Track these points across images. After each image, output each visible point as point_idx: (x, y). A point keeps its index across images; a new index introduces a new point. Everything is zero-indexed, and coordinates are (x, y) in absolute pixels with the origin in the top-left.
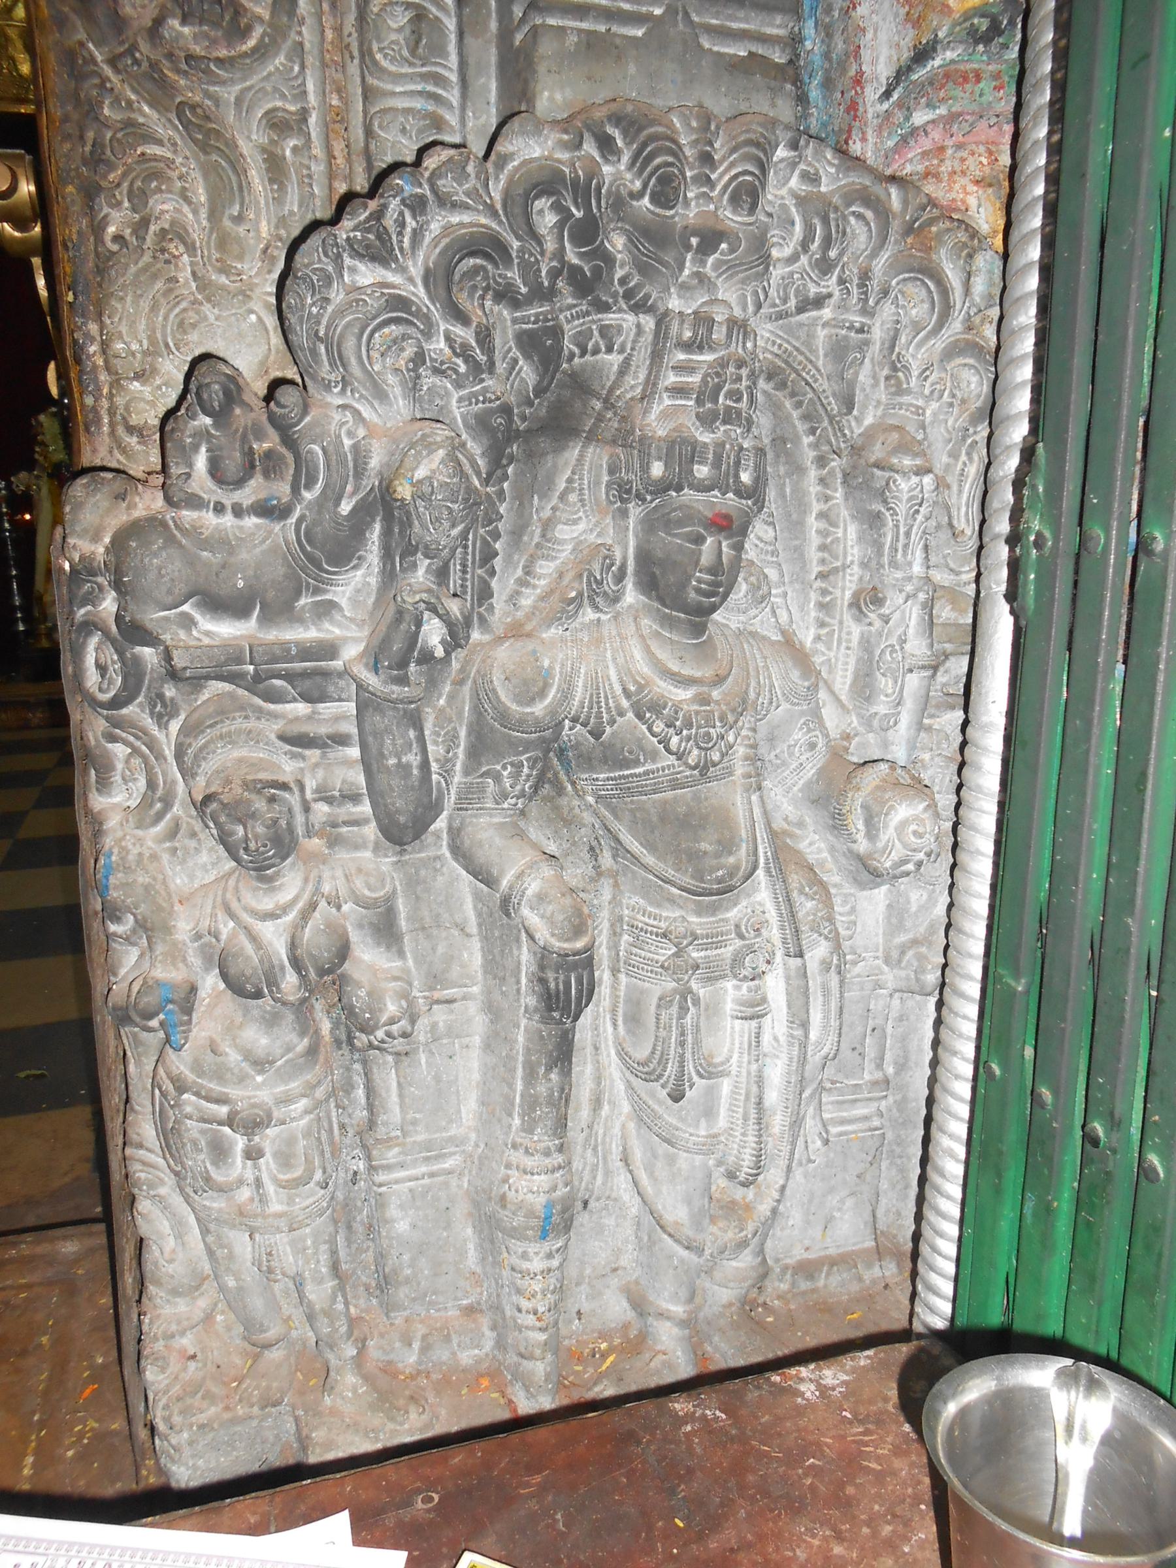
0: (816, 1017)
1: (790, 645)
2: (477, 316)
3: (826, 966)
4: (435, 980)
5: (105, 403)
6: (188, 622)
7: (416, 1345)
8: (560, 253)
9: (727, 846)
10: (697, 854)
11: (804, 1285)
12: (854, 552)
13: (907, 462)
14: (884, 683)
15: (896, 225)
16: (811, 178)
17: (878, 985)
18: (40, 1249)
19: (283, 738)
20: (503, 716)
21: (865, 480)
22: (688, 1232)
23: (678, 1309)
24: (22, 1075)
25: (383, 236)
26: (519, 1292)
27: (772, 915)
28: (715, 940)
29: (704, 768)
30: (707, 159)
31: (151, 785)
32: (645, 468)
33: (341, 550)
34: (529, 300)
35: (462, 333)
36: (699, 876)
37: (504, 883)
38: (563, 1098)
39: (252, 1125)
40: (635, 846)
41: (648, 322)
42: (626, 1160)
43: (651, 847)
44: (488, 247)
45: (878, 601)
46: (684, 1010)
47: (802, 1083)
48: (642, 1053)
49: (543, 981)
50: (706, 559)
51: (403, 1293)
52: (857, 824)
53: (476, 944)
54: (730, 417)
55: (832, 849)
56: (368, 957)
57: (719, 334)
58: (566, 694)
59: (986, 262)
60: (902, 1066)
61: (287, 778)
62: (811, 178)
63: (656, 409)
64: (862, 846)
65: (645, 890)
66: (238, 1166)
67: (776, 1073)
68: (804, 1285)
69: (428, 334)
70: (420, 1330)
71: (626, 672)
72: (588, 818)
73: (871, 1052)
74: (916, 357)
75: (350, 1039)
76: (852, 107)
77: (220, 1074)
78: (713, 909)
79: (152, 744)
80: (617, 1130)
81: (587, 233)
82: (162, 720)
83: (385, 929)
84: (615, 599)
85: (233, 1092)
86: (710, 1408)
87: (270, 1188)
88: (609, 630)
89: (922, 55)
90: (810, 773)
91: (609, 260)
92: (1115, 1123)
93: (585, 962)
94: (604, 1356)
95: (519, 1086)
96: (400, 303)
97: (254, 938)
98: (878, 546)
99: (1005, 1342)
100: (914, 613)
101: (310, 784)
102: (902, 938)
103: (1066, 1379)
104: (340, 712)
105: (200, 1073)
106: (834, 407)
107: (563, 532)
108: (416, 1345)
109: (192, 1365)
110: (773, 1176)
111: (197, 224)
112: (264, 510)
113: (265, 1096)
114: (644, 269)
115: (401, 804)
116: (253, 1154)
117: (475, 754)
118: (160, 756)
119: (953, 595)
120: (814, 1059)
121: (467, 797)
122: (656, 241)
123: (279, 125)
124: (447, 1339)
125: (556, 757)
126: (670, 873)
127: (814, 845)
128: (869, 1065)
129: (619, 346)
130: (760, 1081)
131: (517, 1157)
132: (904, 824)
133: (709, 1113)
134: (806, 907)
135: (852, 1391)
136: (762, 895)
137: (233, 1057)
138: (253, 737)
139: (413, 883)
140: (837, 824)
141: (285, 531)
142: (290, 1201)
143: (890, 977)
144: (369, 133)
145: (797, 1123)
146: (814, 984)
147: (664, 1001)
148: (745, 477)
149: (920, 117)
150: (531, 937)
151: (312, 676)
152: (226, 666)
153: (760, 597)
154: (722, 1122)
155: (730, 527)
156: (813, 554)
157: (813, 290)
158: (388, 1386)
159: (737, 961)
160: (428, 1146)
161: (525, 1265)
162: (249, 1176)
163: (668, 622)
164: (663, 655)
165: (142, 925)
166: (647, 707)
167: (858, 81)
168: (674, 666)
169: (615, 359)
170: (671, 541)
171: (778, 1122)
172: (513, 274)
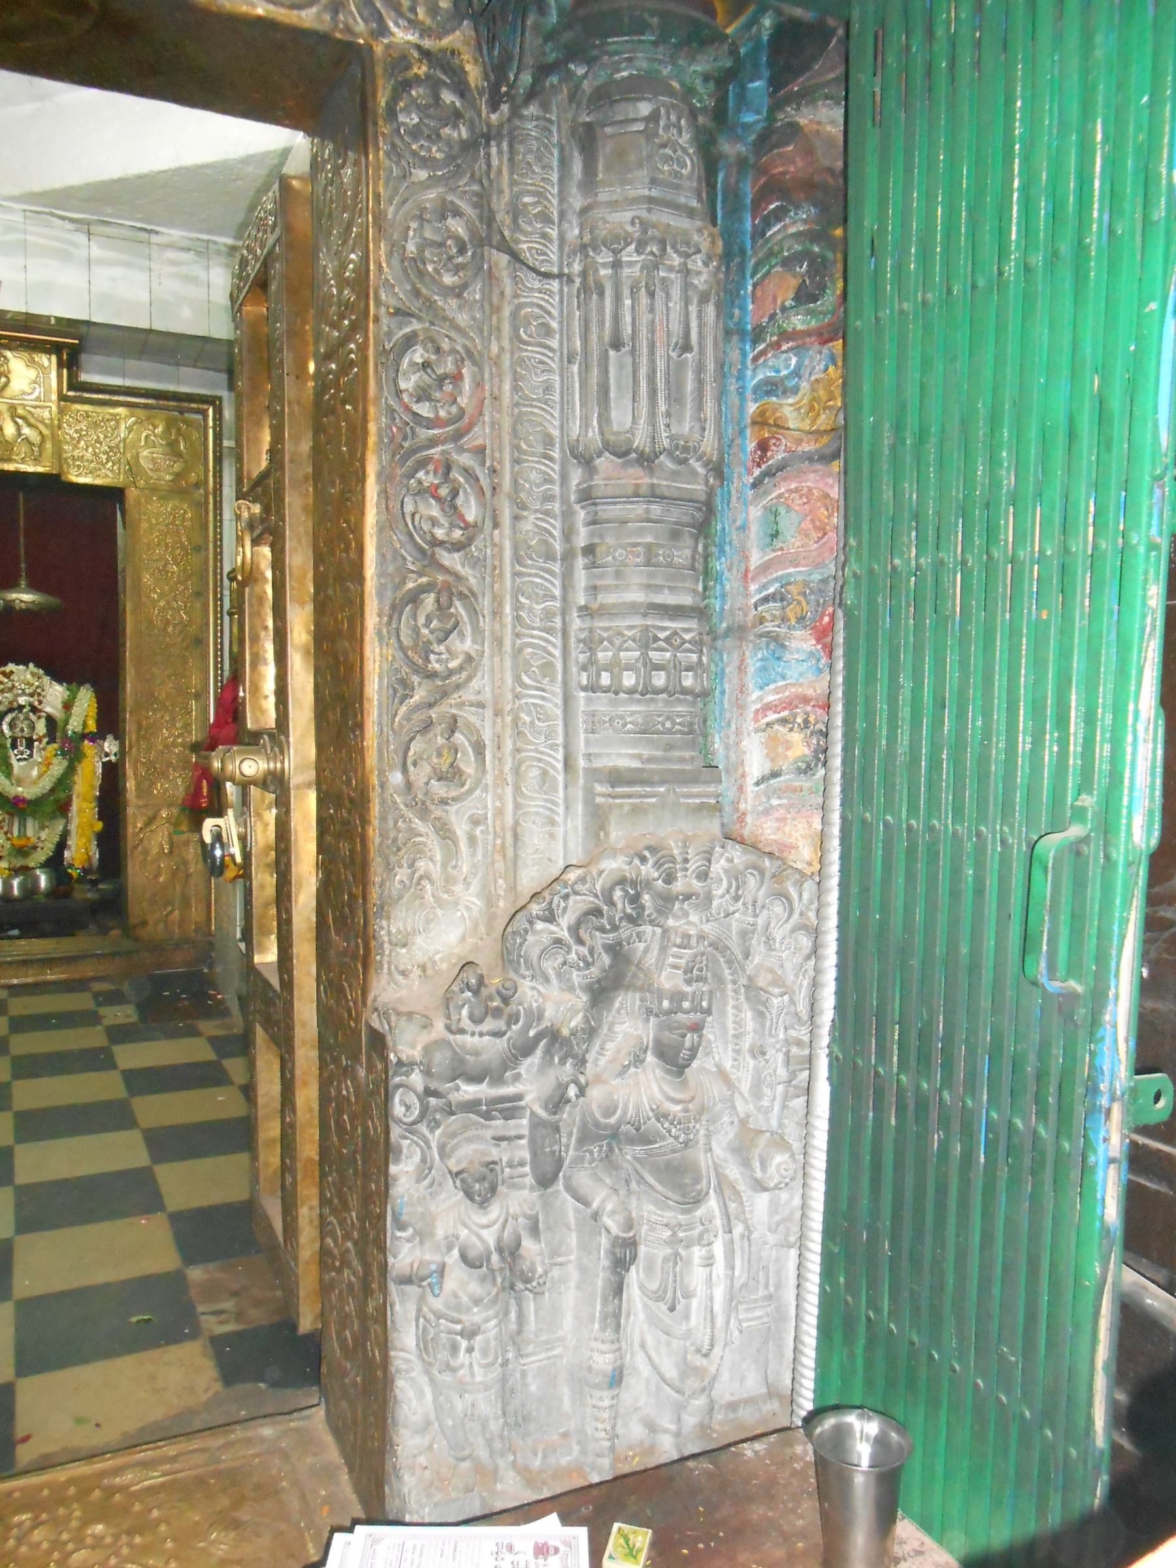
0: (738, 1263)
1: (722, 1074)
2: (588, 941)
3: (742, 1237)
4: (555, 1253)
5: (386, 959)
6: (458, 1089)
7: (540, 1455)
8: (624, 910)
9: (697, 1180)
10: (682, 1182)
11: (732, 1416)
12: (750, 1025)
13: (776, 991)
14: (767, 1091)
15: (768, 874)
16: (730, 860)
17: (765, 1243)
18: (249, 1434)
19: (494, 1138)
20: (597, 1124)
21: (754, 993)
22: (677, 1383)
23: (673, 1427)
24: (134, 1319)
25: (552, 912)
26: (597, 1419)
27: (717, 1213)
28: (690, 1227)
29: (686, 1144)
30: (686, 861)
31: (424, 1160)
32: (660, 1003)
33: (526, 1050)
34: (610, 931)
35: (584, 950)
36: (684, 1196)
37: (595, 1205)
38: (617, 1315)
39: (470, 1333)
40: (651, 1181)
41: (659, 930)
42: (643, 1346)
43: (661, 1182)
44: (597, 912)
45: (763, 1053)
46: (676, 1263)
47: (731, 1300)
48: (654, 1286)
49: (614, 1253)
50: (688, 1044)
51: (532, 1426)
52: (757, 1164)
53: (574, 1235)
54: (699, 979)
55: (742, 1174)
56: (528, 1244)
57: (693, 942)
58: (625, 1112)
59: (809, 887)
60: (778, 1286)
61: (496, 1159)
62: (730, 860)
63: (664, 973)
64: (759, 1174)
65: (656, 1203)
66: (462, 1356)
67: (719, 1294)
68: (732, 1416)
69: (569, 952)
70: (541, 1447)
71: (651, 1098)
72: (625, 1165)
73: (762, 1279)
74: (778, 934)
75: (512, 1287)
76: (741, 788)
77: (458, 1308)
78: (688, 1211)
79: (427, 1142)
80: (637, 1330)
81: (635, 900)
82: (432, 1130)
83: (535, 1231)
84: (643, 1061)
85: (464, 1317)
86: (706, 1465)
87: (476, 1368)
88: (642, 1077)
89: (775, 774)
90: (731, 1136)
91: (643, 908)
92: (878, 1311)
93: (632, 1244)
94: (633, 1457)
95: (599, 1307)
96: (558, 942)
97: (479, 1237)
98: (763, 1026)
99: (837, 1408)
100: (780, 1057)
101: (505, 1159)
102: (777, 1218)
103: (861, 1417)
104: (523, 1124)
105: (449, 1308)
106: (740, 957)
107: (618, 1028)
108: (540, 1455)
109: (427, 1472)
110: (717, 1351)
111: (436, 871)
112: (498, 1034)
113: (477, 1319)
114: (659, 912)
115: (549, 1168)
116: (470, 1350)
117: (581, 1142)
118: (429, 1147)
119: (799, 1043)
120: (737, 1285)
121: (578, 1161)
122: (666, 901)
123: (475, 822)
124: (555, 1451)
125: (609, 1137)
126: (670, 1194)
127: (733, 1172)
128: (761, 1288)
129: (646, 944)
130: (711, 1299)
131: (595, 1345)
132: (779, 1166)
133: (687, 1317)
134: (733, 1206)
135: (769, 1452)
136: (712, 1203)
137: (465, 1299)
138: (481, 1139)
139: (546, 1205)
140: (746, 1163)
141: (501, 1044)
142: (486, 1375)
143: (772, 1239)
144: (517, 823)
145: (728, 1322)
146: (737, 1246)
147: (666, 1260)
148: (704, 1004)
149: (775, 802)
150: (608, 1231)
151: (509, 1108)
152: (472, 1106)
153: (708, 1053)
154: (693, 1321)
155: (697, 1028)
156: (730, 1025)
157: (731, 909)
158: (529, 1477)
159: (701, 1237)
160: (547, 1342)
161: (601, 1404)
162: (467, 1363)
163: (668, 1072)
164: (666, 1088)
165: (418, 1233)
166: (661, 1116)
167: (743, 776)
168: (672, 1094)
169: (642, 946)
170: (670, 1037)
171: (720, 1321)
172: (604, 921)
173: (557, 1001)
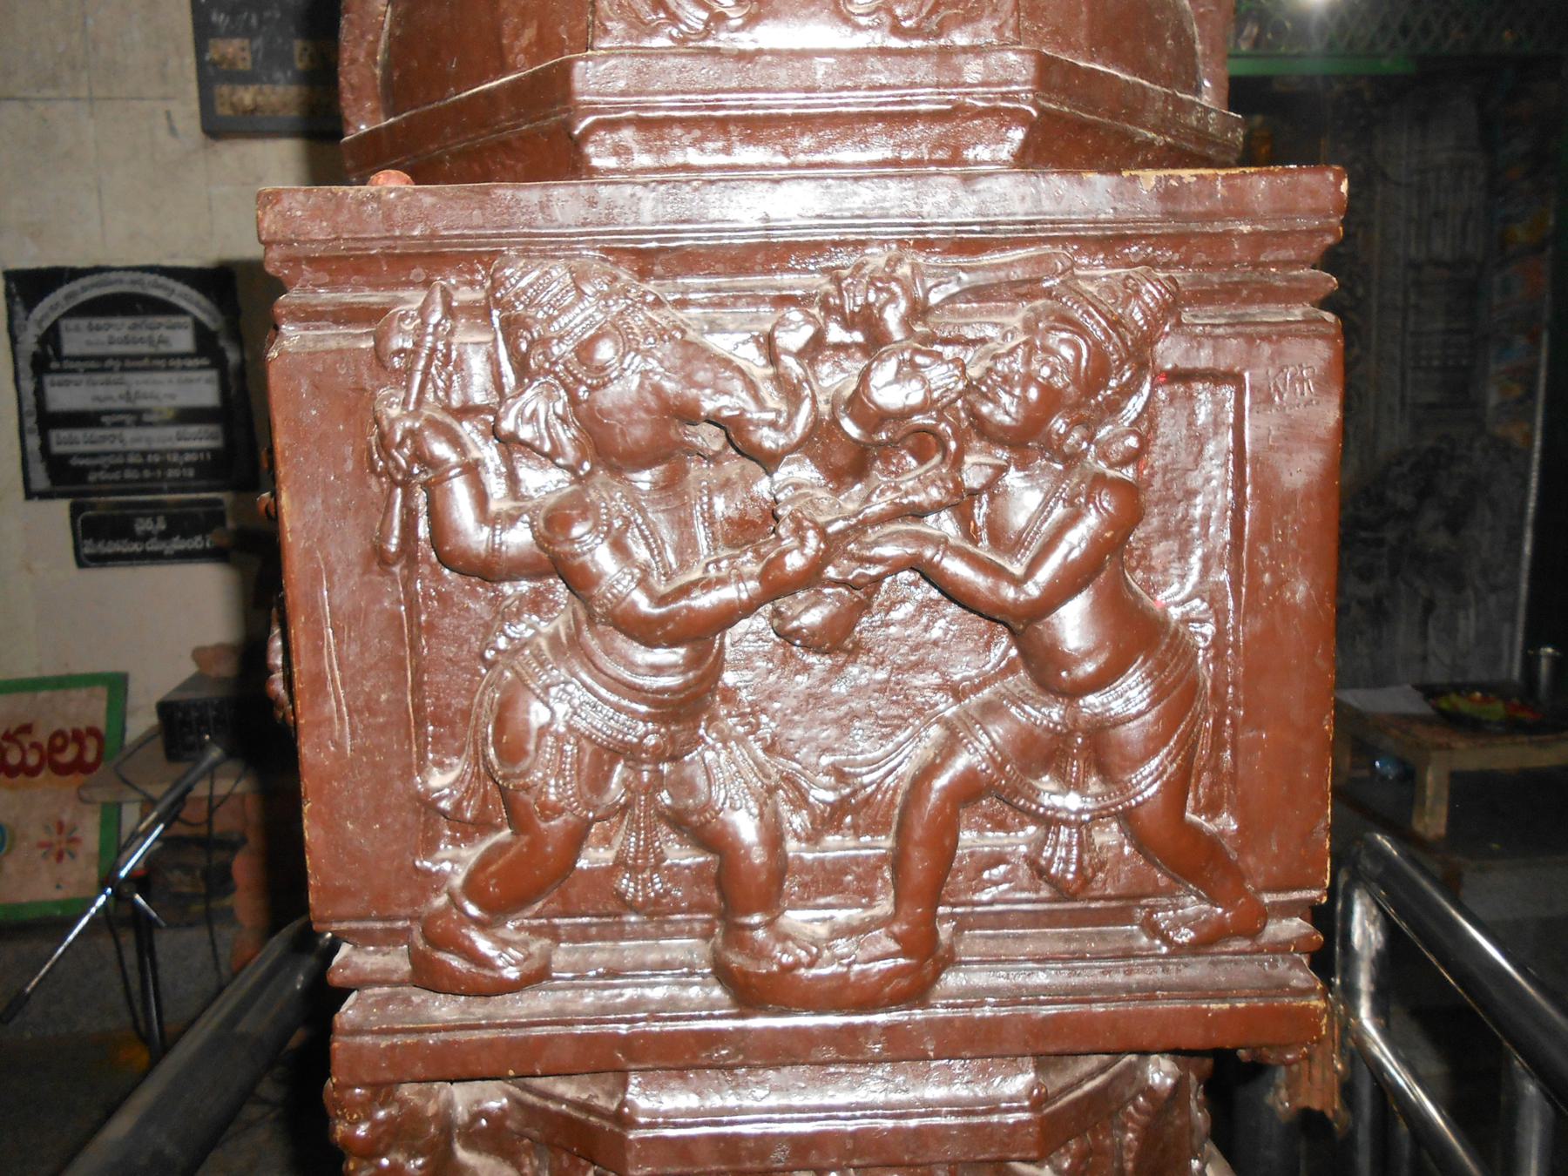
10: (1457, 581)
151: (1380, 543)
173: (1404, 500)
